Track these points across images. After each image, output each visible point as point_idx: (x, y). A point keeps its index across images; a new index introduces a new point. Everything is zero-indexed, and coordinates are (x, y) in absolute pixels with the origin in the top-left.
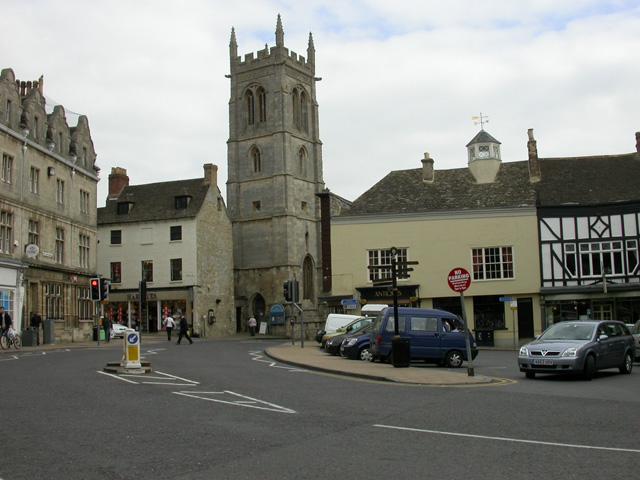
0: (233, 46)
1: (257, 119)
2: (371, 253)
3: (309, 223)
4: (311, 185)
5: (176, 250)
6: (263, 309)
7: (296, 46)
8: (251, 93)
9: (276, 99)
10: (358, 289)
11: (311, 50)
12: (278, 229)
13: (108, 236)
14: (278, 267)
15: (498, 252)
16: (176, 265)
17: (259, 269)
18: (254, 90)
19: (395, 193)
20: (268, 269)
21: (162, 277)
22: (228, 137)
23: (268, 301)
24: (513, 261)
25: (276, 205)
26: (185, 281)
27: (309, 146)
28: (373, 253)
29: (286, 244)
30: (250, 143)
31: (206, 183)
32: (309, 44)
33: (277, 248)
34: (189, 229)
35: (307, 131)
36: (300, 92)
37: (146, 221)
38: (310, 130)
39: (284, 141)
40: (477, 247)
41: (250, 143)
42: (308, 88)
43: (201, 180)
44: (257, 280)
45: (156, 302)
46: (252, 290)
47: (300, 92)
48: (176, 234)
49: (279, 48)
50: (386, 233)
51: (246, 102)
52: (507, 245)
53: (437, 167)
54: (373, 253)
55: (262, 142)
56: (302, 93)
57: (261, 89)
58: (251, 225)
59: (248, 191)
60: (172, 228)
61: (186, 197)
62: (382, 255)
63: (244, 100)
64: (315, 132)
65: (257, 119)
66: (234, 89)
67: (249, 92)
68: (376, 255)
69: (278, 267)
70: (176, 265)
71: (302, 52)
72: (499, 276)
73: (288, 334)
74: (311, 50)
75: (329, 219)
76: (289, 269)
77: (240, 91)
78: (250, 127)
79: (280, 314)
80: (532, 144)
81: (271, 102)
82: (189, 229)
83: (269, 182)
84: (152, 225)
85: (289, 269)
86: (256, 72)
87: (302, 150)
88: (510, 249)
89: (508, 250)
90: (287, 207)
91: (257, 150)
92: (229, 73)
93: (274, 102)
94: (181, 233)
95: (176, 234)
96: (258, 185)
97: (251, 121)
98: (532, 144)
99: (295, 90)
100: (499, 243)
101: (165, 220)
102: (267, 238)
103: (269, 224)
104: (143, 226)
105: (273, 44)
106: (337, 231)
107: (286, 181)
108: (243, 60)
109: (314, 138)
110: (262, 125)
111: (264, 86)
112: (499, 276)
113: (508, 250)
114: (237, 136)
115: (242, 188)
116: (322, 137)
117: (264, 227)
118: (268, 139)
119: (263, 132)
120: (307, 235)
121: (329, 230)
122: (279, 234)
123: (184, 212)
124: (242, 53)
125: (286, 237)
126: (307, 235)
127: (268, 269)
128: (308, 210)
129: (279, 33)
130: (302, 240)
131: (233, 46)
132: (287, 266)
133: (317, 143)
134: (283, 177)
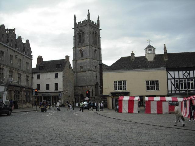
0: (75, 19)
7: (94, 19)
10: (110, 93)
11: (98, 21)
14: (88, 86)
16: (56, 85)
18: (81, 33)
26: (59, 90)
30: (80, 48)
34: (61, 74)
35: (97, 45)
37: (48, 72)
40: (116, 80)
41: (80, 48)
47: (95, 33)
48: (57, 76)
52: (124, 80)
55: (83, 48)
57: (83, 33)
60: (55, 74)
62: (151, 82)
63: (77, 37)
65: (82, 41)
66: (75, 32)
69: (88, 86)
70: (56, 85)
71: (95, 21)
72: (122, 90)
74: (98, 21)
77: (77, 33)
81: (86, 36)
82: (61, 74)
83: (85, 60)
84: (50, 73)
87: (95, 51)
88: (158, 81)
91: (82, 51)
95: (57, 76)
100: (154, 79)
101: (53, 72)
103: (85, 73)
108: (78, 24)
112: (122, 90)
117: (84, 74)
118: (85, 47)
120: (97, 76)
124: (77, 22)
126: (97, 76)
127: (84, 86)
129: (89, 16)
131: (75, 19)
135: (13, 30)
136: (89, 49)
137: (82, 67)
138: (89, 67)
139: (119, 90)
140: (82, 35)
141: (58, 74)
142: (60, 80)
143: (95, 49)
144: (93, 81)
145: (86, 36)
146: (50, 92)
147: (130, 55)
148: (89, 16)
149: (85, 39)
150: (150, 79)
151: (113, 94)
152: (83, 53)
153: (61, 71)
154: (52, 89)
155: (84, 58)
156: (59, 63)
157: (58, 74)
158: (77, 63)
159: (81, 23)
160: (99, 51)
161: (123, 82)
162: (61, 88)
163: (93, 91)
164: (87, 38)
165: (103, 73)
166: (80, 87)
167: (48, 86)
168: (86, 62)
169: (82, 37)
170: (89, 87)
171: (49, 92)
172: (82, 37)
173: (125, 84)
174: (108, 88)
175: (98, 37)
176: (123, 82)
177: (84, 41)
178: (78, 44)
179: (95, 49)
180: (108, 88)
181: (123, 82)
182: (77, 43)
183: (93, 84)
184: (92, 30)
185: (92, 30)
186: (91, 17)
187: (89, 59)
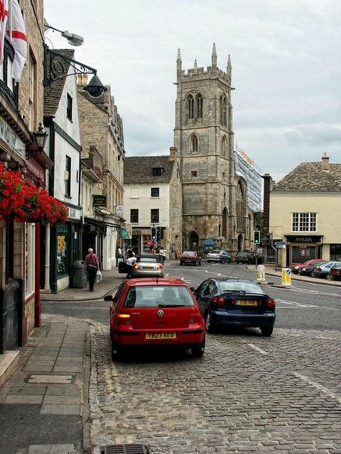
0: (179, 62)
1: (195, 115)
2: (294, 214)
4: (228, 162)
6: (197, 242)
7: (222, 66)
8: (191, 97)
9: (211, 104)
10: (286, 236)
13: (150, 191)
14: (210, 216)
15: (308, 216)
16: (155, 213)
17: (194, 216)
19: (306, 177)
20: (201, 216)
21: (145, 220)
23: (201, 237)
24: (316, 222)
25: (209, 175)
26: (161, 224)
27: (227, 134)
28: (295, 215)
30: (191, 131)
31: (171, 159)
32: (228, 64)
33: (209, 203)
34: (165, 190)
35: (225, 125)
38: (228, 124)
40: (296, 211)
41: (191, 131)
42: (227, 95)
43: (167, 157)
46: (190, 228)
48: (155, 193)
49: (214, 66)
50: (304, 203)
52: (313, 211)
53: (330, 161)
54: (295, 215)
55: (199, 132)
57: (199, 95)
61: (160, 169)
62: (301, 216)
63: (184, 104)
65: (195, 115)
66: (179, 93)
68: (297, 216)
69: (210, 216)
70: (155, 213)
71: (225, 71)
72: (307, 230)
74: (229, 67)
77: (184, 95)
79: (212, 246)
82: (165, 190)
83: (204, 159)
84: (139, 186)
85: (217, 217)
87: (224, 138)
88: (315, 214)
89: (314, 215)
90: (216, 176)
91: (195, 137)
95: (155, 193)
96: (196, 160)
97: (191, 116)
99: (221, 97)
100: (310, 210)
101: (148, 183)
107: (216, 159)
108: (186, 73)
109: (230, 129)
110: (200, 119)
111: (202, 93)
112: (307, 230)
113: (314, 215)
116: (233, 130)
117: (201, 189)
118: (204, 130)
121: (269, 199)
122: (211, 194)
123: (160, 179)
124: (187, 66)
127: (201, 216)
129: (214, 57)
130: (222, 198)
131: (179, 62)
132: (216, 215)
133: (231, 133)
135: (103, 87)
137: (194, 174)
138: (213, 175)
139: (301, 230)
144: (220, 204)
145: (207, 104)
146: (139, 226)
147: (168, 153)
148: (214, 57)
149: (205, 112)
150: (300, 211)
151: (290, 238)
152: (199, 141)
154: (145, 220)
155: (200, 154)
159: (205, 70)
161: (299, 215)
162: (164, 221)
163: (220, 226)
164: (210, 109)
169: (195, 105)
170: (213, 217)
171: (137, 228)
172: (195, 105)
173: (313, 220)
174: (280, 226)
176: (299, 215)
177: (200, 114)
179: (223, 133)
180: (280, 226)
181: (311, 214)
182: (184, 119)
183: (220, 211)
184: (218, 91)
185: (218, 91)
186: (218, 59)
187: (213, 158)
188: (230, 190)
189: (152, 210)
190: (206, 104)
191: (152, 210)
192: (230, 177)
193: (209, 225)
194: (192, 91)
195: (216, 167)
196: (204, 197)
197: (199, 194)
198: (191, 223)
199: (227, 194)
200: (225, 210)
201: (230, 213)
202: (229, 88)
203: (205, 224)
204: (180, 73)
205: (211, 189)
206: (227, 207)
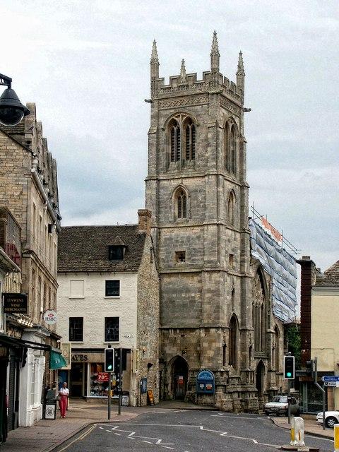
0: (155, 64)
1: (183, 155)
3: (235, 278)
4: (238, 235)
5: (112, 308)
7: (228, 71)
9: (210, 135)
11: (241, 73)
12: (208, 285)
14: (207, 329)
16: (112, 325)
17: (181, 329)
18: (180, 121)
21: (94, 336)
22: (146, 175)
23: (192, 366)
26: (123, 343)
29: (218, 303)
31: (141, 231)
33: (206, 307)
34: (129, 284)
35: (234, 172)
36: (231, 125)
37: (76, 272)
39: (218, 185)
41: (175, 183)
42: (237, 120)
43: (134, 227)
44: (179, 341)
45: (86, 364)
46: (172, 351)
47: (231, 125)
48: (113, 289)
51: (170, 135)
55: (190, 184)
56: (233, 126)
57: (189, 121)
58: (173, 279)
59: (171, 239)
60: (106, 281)
61: (122, 247)
63: (164, 135)
64: (242, 173)
65: (183, 155)
66: (155, 117)
67: (174, 123)
69: (207, 329)
70: (112, 325)
73: (218, 405)
74: (241, 73)
75: (310, 288)
76: (220, 332)
77: (162, 121)
78: (174, 165)
79: (210, 381)
80: (183, 67)
81: (202, 137)
82: (129, 284)
83: (197, 230)
86: (185, 99)
87: (232, 194)
90: (219, 260)
91: (182, 192)
92: (149, 98)
93: (206, 140)
94: (119, 288)
95: (113, 289)
96: (183, 233)
97: (174, 157)
98: (183, 67)
99: (227, 125)
101: (100, 272)
102: (193, 295)
103: (196, 278)
104: (72, 278)
105: (208, 68)
106: (317, 299)
107: (219, 231)
108: (167, 83)
109: (241, 179)
110: (189, 163)
111: (194, 117)
114: (158, 173)
115: (162, 235)
117: (192, 282)
118: (198, 181)
119: (191, 172)
120: (233, 292)
122: (209, 291)
123: (121, 265)
124: (168, 71)
125: (219, 295)
126: (233, 292)
128: (234, 264)
129: (215, 56)
130: (229, 297)
131: (155, 64)
132: (218, 328)
133: (244, 187)
134: (215, 227)
136: (214, 189)
137: (181, 256)
140: (182, 131)
141: (118, 281)
142: (127, 306)
143: (229, 186)
144: (225, 308)
145: (202, 137)
147: (134, 220)
148: (215, 56)
149: (199, 149)
152: (188, 200)
153: (134, 270)
154: (94, 336)
155: (191, 223)
156: (118, 240)
157: (118, 281)
158: (162, 239)
159: (200, 78)
160: (242, 195)
165: (313, 292)
166: (175, 329)
167: (76, 326)
168: (198, 237)
170: (213, 331)
175: (238, 141)
177: (191, 154)
178: (168, 165)
179: (229, 186)
184: (222, 114)
185: (222, 114)
187: (213, 229)
188: (242, 283)
189: (71, 319)
190: (201, 135)
191: (71, 319)
192: (243, 261)
193: (205, 345)
194: (177, 114)
195: (219, 245)
196: (197, 296)
197: (188, 291)
198: (174, 342)
199: (238, 291)
200: (233, 319)
201: (243, 323)
202: (240, 109)
203: (199, 343)
204: (156, 82)
205: (209, 282)
206: (238, 314)
